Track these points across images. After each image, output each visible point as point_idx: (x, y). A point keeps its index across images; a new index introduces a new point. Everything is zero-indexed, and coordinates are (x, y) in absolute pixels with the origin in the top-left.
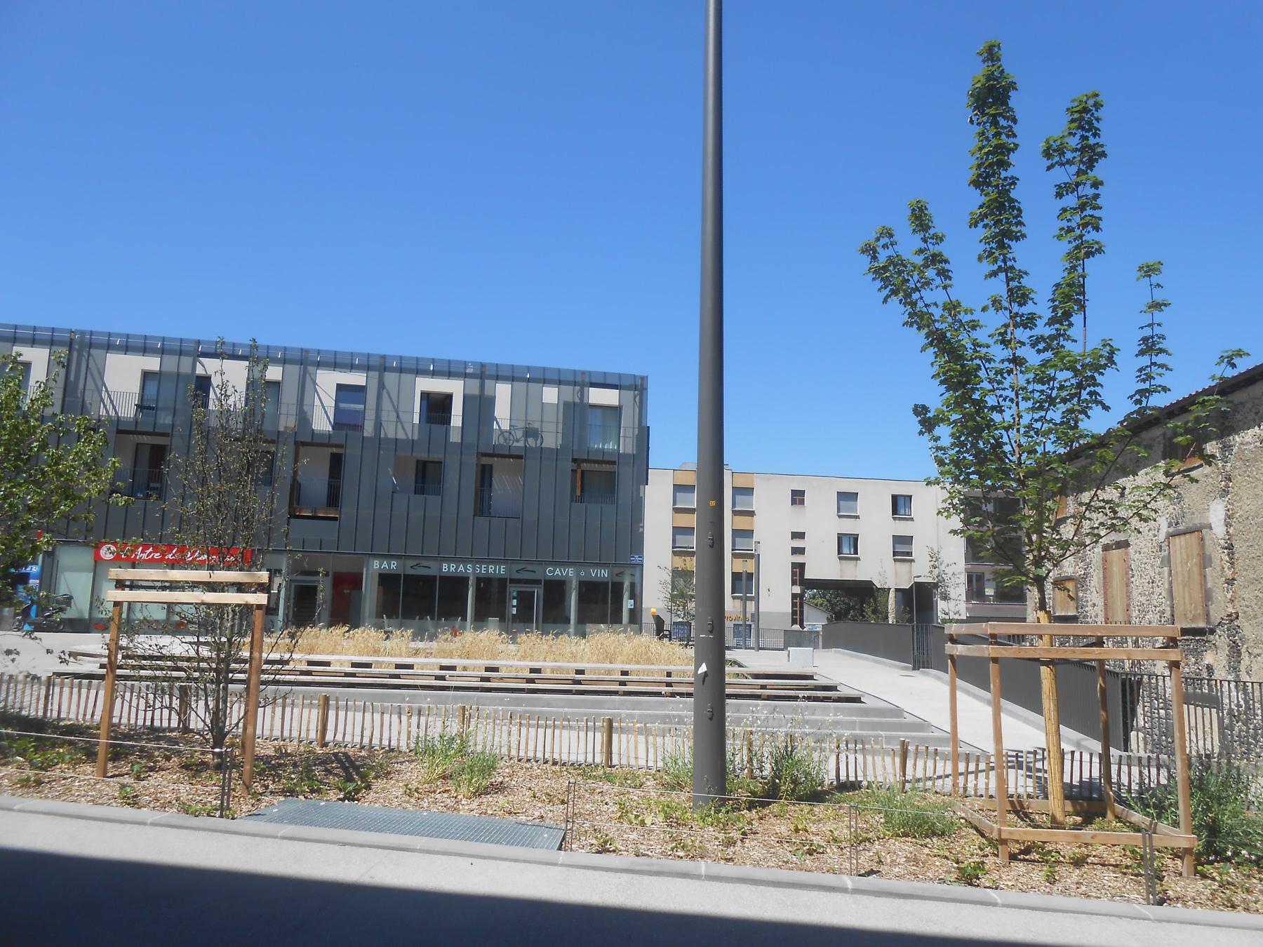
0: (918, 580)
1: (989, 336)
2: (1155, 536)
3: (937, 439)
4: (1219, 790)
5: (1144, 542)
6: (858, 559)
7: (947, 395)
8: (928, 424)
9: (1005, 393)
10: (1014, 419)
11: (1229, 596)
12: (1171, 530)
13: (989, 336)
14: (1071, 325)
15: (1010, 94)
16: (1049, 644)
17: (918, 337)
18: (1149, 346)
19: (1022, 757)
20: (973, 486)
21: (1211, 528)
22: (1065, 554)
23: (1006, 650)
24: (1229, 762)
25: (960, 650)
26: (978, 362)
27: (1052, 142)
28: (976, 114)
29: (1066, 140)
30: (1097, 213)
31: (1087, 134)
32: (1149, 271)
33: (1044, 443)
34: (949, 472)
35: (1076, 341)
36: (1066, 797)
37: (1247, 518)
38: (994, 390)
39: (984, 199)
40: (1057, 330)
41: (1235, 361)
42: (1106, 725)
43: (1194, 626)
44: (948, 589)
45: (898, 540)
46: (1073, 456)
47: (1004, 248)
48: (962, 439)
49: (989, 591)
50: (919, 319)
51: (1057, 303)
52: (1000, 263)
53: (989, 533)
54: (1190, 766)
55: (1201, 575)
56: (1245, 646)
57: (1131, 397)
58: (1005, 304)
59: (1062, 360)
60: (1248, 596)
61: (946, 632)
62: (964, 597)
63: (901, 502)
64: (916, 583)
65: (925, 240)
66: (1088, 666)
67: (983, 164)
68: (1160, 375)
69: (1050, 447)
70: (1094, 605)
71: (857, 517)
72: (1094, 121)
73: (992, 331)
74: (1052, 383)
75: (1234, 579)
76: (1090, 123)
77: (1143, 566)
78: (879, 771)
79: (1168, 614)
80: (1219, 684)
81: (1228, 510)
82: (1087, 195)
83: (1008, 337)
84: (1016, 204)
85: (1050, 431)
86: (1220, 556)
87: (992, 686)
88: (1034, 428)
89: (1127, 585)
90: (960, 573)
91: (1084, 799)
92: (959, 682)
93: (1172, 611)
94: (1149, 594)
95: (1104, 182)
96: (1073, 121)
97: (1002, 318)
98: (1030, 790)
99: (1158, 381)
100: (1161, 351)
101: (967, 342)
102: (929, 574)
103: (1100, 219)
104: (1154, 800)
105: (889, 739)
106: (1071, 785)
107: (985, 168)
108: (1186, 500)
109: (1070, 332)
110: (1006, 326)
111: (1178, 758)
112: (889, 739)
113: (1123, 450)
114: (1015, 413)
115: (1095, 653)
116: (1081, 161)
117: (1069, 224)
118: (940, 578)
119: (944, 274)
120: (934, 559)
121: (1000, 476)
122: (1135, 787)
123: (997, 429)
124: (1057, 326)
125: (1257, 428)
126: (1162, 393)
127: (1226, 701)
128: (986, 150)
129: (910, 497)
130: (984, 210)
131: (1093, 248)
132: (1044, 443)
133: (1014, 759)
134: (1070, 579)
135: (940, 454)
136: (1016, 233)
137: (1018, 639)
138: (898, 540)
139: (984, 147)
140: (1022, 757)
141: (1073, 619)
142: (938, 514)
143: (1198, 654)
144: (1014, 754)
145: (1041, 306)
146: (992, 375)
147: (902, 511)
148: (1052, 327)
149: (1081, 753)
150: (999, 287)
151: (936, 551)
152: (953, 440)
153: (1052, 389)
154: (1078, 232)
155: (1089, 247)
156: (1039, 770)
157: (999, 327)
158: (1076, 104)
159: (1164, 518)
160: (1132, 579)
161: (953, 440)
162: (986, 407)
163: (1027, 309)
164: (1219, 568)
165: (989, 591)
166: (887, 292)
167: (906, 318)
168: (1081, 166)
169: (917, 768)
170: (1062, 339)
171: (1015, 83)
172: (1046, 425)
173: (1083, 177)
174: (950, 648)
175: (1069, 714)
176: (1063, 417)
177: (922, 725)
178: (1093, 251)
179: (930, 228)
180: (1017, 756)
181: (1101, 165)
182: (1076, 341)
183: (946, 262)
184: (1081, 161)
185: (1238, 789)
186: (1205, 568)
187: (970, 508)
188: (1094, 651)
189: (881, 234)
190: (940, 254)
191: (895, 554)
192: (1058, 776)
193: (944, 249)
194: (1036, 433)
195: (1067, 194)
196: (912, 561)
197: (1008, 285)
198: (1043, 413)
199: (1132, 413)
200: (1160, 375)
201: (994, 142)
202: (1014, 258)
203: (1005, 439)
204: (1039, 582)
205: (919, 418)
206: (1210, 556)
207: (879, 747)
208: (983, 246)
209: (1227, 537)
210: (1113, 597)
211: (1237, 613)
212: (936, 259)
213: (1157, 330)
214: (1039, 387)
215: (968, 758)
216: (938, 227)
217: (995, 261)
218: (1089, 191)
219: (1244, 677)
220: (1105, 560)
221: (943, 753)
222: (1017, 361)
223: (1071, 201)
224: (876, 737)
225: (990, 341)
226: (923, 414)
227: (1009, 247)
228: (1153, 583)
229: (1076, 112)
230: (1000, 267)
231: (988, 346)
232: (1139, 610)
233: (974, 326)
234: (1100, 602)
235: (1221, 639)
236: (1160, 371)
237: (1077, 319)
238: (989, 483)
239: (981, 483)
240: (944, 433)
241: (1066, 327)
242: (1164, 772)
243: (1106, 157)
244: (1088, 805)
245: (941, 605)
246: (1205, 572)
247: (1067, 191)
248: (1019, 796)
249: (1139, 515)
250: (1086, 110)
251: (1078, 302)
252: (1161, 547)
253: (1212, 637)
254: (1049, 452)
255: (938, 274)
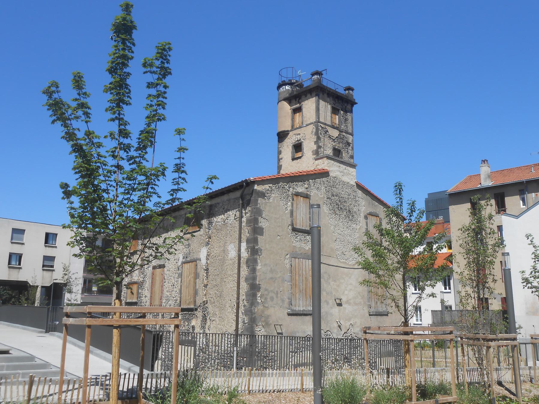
0: (55, 281)
1: (106, 152)
2: (177, 263)
3: (72, 203)
4: (190, 387)
5: (172, 266)
6: (20, 268)
7: (79, 180)
8: (68, 194)
9: (111, 183)
10: (114, 197)
11: (205, 293)
12: (184, 260)
13: (106, 152)
14: (146, 153)
15: (133, 31)
16: (119, 317)
17: (68, 146)
18: (179, 168)
19: (99, 379)
20: (88, 231)
21: (200, 260)
22: (132, 270)
23: (95, 321)
24: (196, 372)
25: (71, 321)
26: (99, 164)
27: (147, 61)
28: (114, 36)
29: (154, 61)
30: (164, 100)
31: (164, 61)
32: (179, 132)
33: (128, 211)
34: (76, 222)
35: (148, 161)
36: (119, 398)
37: (215, 257)
38: (105, 181)
39: (113, 80)
40: (140, 154)
41: (213, 180)
42: (143, 357)
43: (189, 307)
44: (72, 287)
45: (46, 258)
46: (142, 221)
47: (120, 108)
48: (85, 205)
49: (95, 289)
50: (70, 136)
51: (140, 140)
52: (116, 115)
53: (94, 257)
54: (178, 376)
55: (194, 283)
56: (209, 316)
57: (169, 192)
58: (117, 137)
59: (141, 170)
60: (212, 293)
61: (64, 311)
62: (80, 292)
63: (51, 237)
64: (54, 283)
65: (79, 94)
66: (138, 328)
67: (114, 62)
68: (182, 183)
69: (130, 214)
70: (146, 296)
71: (23, 244)
72: (168, 56)
73: (108, 149)
74: (135, 181)
75: (207, 285)
76: (166, 56)
77: (170, 277)
78: (15, 394)
79: (178, 301)
80: (196, 335)
81: (208, 252)
82: (161, 91)
83: (116, 155)
84: (128, 87)
85: (131, 205)
86: (202, 273)
87: (86, 341)
88: (124, 203)
89: (162, 287)
90: (80, 278)
91: (128, 398)
92: (69, 338)
93: (180, 300)
94: (171, 291)
95: (169, 86)
96: (158, 53)
97: (115, 144)
98: (101, 397)
99: (181, 186)
100: (183, 172)
101: (94, 152)
102: (62, 279)
103: (166, 104)
104: (161, 395)
105: (24, 375)
106: (123, 391)
107: (115, 64)
108: (192, 246)
109: (146, 156)
110: (116, 148)
111: (173, 372)
112: (24, 375)
113: (164, 218)
114: (115, 194)
115: (141, 321)
116: (160, 74)
117: (151, 103)
118: (68, 281)
119: (87, 114)
120: (66, 270)
121: (103, 226)
122: (153, 389)
123: (104, 201)
124: (140, 152)
125: (223, 215)
126: (183, 191)
127: (198, 343)
128: (117, 55)
129: (56, 235)
130: (112, 86)
131: (161, 117)
132: (128, 211)
133: (95, 380)
134: (135, 283)
135: (72, 211)
136: (127, 101)
137: (105, 315)
138: (46, 258)
139: (116, 53)
140: (99, 379)
141: (135, 304)
142: (67, 245)
143: (189, 320)
144: (95, 377)
145: (133, 141)
146: (105, 172)
147: (51, 242)
148: (137, 152)
149: (129, 374)
150: (115, 127)
151: (67, 265)
152: (81, 205)
153: (135, 184)
154: (155, 108)
155: (159, 116)
156: (107, 385)
157: (112, 148)
158: (160, 45)
159: (181, 254)
160: (165, 284)
161: (81, 205)
162: (100, 189)
163: (126, 141)
164: (202, 280)
165: (95, 289)
166: (54, 118)
167: (63, 134)
168: (160, 76)
169: (39, 390)
170: (141, 159)
171: (136, 27)
172: (130, 202)
173: (160, 82)
174: (66, 320)
175: (124, 354)
176: (139, 200)
177: (46, 365)
178: (161, 118)
179: (83, 88)
180: (96, 379)
181: (168, 77)
182: (148, 161)
183: (89, 108)
184: (160, 74)
185: (198, 385)
186: (196, 279)
187: (90, 242)
188: (140, 320)
189: (52, 85)
190: (86, 103)
191: (43, 266)
192: (116, 387)
193: (88, 101)
194: (124, 206)
195: (152, 88)
196: (53, 270)
197: (119, 127)
198: (129, 196)
199: (169, 200)
200: (182, 183)
201: (122, 52)
202: (124, 114)
203: (108, 207)
204: (119, 284)
205: (63, 190)
206: (199, 273)
207: (16, 380)
208: (109, 104)
209: (207, 265)
210: (155, 292)
211: (207, 301)
212: (82, 106)
213: (182, 161)
214: (128, 182)
215: (69, 382)
216: (87, 89)
217: (114, 113)
218: (163, 90)
219: (207, 331)
220: (153, 274)
221: (55, 381)
222: (119, 167)
223: (153, 91)
224: (15, 374)
225: (107, 155)
226: (65, 188)
227: (122, 108)
228: (173, 286)
229: (160, 49)
230: (116, 117)
231: (105, 157)
232: (166, 299)
233: (99, 145)
234: (149, 295)
235: (199, 314)
236: (182, 181)
237: (149, 150)
238: (97, 230)
239: (93, 230)
240: (76, 200)
241: (144, 154)
242: (167, 380)
243: (171, 75)
244: (130, 402)
245: (67, 296)
246: (196, 281)
247: (152, 86)
248: (95, 401)
249: (169, 251)
250: (164, 49)
251: (151, 142)
252: (179, 268)
253: (196, 312)
254: (130, 216)
255: (84, 114)
